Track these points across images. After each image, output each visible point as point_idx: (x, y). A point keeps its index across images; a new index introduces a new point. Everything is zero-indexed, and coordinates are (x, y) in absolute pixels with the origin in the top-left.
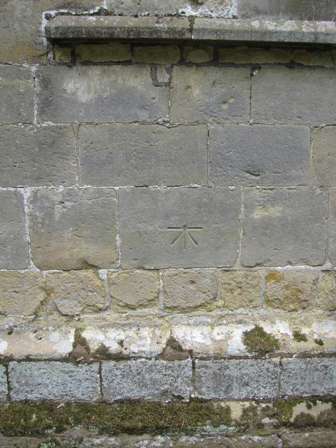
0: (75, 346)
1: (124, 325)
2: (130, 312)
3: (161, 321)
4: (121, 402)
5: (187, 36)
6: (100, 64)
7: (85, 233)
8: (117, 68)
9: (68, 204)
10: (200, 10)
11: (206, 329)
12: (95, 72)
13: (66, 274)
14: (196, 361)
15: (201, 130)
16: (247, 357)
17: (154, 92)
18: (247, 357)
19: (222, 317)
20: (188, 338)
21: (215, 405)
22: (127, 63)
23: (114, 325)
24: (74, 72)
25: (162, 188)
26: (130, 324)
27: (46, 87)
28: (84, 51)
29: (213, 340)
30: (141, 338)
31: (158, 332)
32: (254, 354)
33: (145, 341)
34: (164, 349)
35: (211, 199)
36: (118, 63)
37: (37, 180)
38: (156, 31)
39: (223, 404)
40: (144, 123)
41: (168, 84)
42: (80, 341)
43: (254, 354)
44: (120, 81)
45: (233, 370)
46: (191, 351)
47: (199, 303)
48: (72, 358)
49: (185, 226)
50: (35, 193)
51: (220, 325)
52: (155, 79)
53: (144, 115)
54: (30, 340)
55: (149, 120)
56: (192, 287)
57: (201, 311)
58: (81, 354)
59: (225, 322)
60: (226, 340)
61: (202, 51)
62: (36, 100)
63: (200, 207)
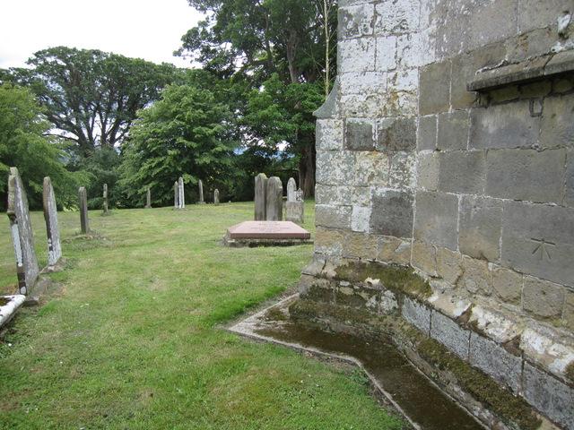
0: (464, 313)
1: (497, 312)
2: (503, 304)
3: (519, 320)
4: (477, 369)
5: (541, 73)
6: (502, 103)
7: (484, 232)
8: (510, 105)
9: (478, 208)
10: (566, 45)
11: (547, 342)
12: (498, 109)
13: (472, 260)
14: (525, 363)
15: (560, 152)
16: (563, 381)
17: (531, 122)
18: (563, 381)
19: (564, 336)
20: (530, 342)
21: (533, 413)
22: (516, 100)
23: (491, 310)
24: (487, 112)
25: (530, 203)
26: (500, 313)
27: (474, 124)
28: (493, 94)
29: (546, 352)
30: (501, 327)
31: (514, 328)
32: (569, 381)
33: (501, 330)
34: (508, 341)
35: (564, 218)
36: (511, 101)
37: (466, 189)
38: (522, 74)
39: (538, 416)
40: (523, 148)
41: (540, 115)
42: (468, 313)
43: (569, 381)
44: (511, 116)
45: (549, 387)
46: (523, 351)
47: (546, 315)
48: (457, 320)
49: (543, 240)
50: (464, 198)
51: (560, 343)
52: (532, 110)
53: (523, 142)
54: (447, 300)
55: (526, 146)
56: (543, 298)
57: (549, 324)
58: (466, 323)
59: (564, 342)
60: (554, 357)
61: (566, 81)
62: (469, 133)
63: (555, 225)
